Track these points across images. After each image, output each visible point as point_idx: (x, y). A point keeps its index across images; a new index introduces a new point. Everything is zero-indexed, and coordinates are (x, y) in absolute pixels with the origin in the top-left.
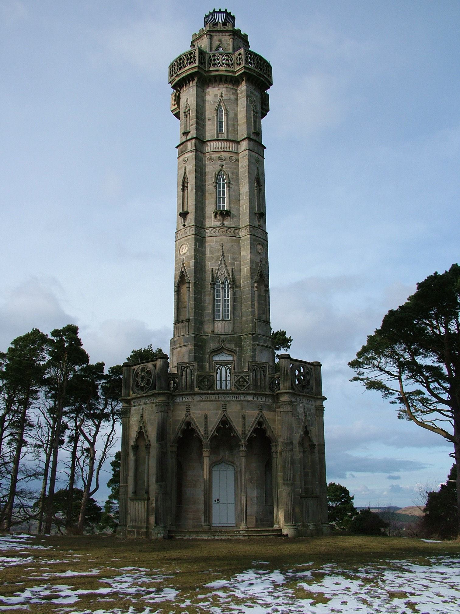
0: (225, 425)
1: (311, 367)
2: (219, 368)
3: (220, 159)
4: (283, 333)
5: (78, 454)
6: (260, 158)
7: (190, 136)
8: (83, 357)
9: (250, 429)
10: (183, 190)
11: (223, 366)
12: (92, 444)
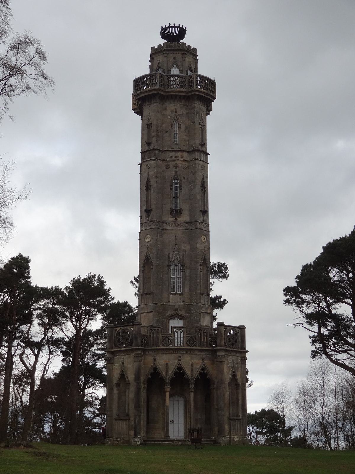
0: (180, 373)
1: (238, 329)
2: (176, 331)
6: (205, 164)
9: (196, 374)
10: (147, 190)
11: (179, 329)
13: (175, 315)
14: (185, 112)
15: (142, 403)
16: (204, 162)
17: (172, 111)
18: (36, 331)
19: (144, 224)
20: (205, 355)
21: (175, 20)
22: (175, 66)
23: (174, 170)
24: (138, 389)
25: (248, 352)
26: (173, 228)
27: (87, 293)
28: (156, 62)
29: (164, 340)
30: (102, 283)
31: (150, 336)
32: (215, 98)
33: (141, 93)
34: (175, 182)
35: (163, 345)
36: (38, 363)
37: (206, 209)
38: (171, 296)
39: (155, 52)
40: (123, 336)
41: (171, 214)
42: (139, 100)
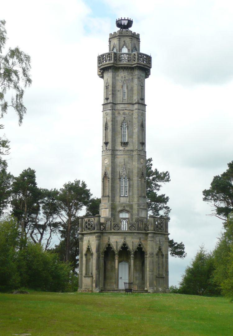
0: (125, 248)
6: (144, 112)
9: (135, 248)
10: (106, 130)
11: (124, 220)
13: (123, 210)
14: (131, 78)
15: (101, 266)
16: (143, 110)
17: (122, 77)
18: (41, 218)
19: (104, 152)
20: (141, 236)
21: (124, 15)
22: (125, 46)
23: (123, 116)
24: (98, 258)
25: (170, 234)
26: (122, 154)
27: (76, 193)
28: (112, 44)
29: (115, 226)
30: (84, 185)
31: (106, 224)
32: (150, 68)
33: (102, 65)
34: (124, 124)
35: (114, 230)
36: (43, 239)
37: (144, 142)
38: (121, 198)
39: (112, 37)
40: (89, 224)
41: (121, 145)
42: (101, 69)
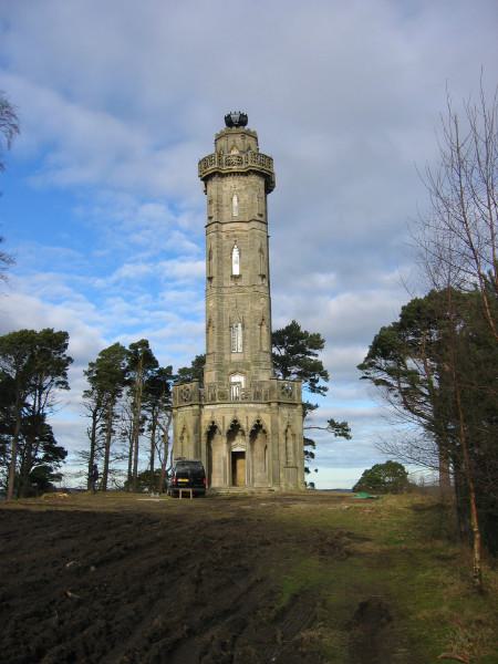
3: (235, 236)
4: (319, 335)
5: (156, 440)
7: (213, 220)
8: (156, 364)
9: (251, 425)
12: (166, 432)
